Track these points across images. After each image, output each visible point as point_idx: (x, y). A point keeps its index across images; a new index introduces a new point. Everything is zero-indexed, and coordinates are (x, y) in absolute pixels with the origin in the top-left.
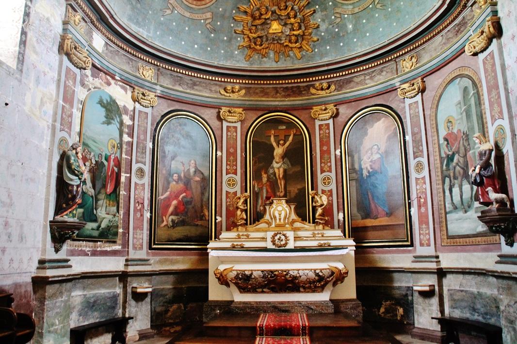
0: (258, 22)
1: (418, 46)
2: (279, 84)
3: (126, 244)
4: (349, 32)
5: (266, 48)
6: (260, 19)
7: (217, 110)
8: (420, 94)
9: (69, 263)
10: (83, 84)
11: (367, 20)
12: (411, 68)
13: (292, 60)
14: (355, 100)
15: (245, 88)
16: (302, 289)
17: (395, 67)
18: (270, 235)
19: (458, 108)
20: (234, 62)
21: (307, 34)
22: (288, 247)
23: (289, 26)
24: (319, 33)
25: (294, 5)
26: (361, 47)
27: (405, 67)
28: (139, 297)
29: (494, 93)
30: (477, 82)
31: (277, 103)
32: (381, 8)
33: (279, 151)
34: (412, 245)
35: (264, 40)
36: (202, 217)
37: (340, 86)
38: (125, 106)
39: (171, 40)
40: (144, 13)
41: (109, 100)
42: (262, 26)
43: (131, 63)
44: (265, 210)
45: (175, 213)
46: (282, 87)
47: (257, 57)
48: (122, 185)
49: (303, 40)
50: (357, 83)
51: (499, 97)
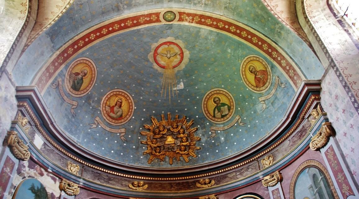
0: (158, 136)
1: (273, 149)
2: (173, 180)
4: (222, 142)
5: (163, 155)
6: (159, 134)
8: (279, 183)
10: (19, 172)
11: (234, 134)
12: (269, 165)
13: (182, 163)
14: (230, 190)
15: (148, 183)
17: (258, 165)
19: (311, 190)
20: (140, 164)
21: (192, 144)
24: (201, 144)
25: (183, 125)
26: (231, 153)
27: (265, 164)
29: (340, 176)
30: (323, 169)
31: (172, 195)
32: (243, 125)
35: (162, 149)
37: (219, 180)
38: (52, 194)
39: (94, 146)
40: (76, 125)
41: (40, 187)
42: (161, 139)
43: (62, 160)
46: (175, 183)
47: (156, 161)
49: (189, 149)
51: (346, 178)
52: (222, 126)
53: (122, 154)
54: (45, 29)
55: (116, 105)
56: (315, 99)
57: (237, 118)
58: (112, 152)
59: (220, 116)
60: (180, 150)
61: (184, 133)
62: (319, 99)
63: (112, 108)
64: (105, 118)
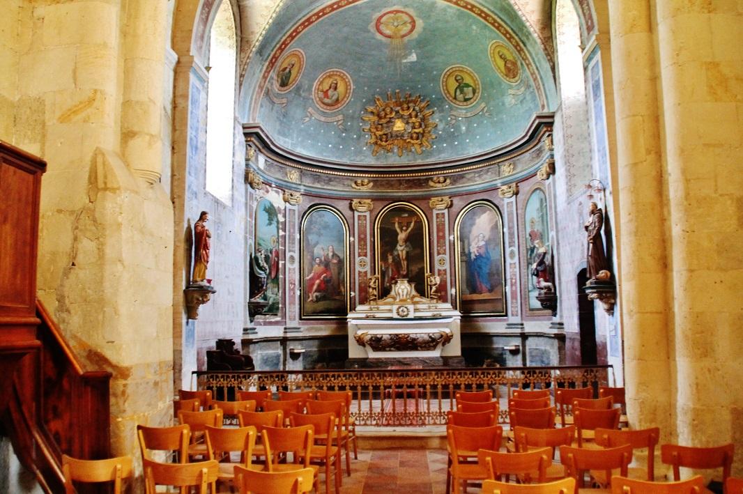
0: (383, 121)
3: (284, 316)
6: (385, 117)
7: (349, 201)
9: (256, 331)
16: (419, 348)
18: (395, 307)
22: (409, 317)
23: (411, 125)
26: (474, 150)
28: (295, 356)
31: (400, 194)
33: (402, 236)
34: (506, 315)
36: (339, 293)
37: (455, 180)
44: (391, 288)
48: (280, 271)
50: (469, 179)
52: (465, 111)
53: (341, 147)
54: (254, 49)
55: (330, 88)
56: (547, 131)
57: (483, 105)
58: (330, 146)
59: (462, 99)
60: (412, 138)
61: (416, 116)
62: (552, 131)
63: (326, 93)
64: (318, 106)
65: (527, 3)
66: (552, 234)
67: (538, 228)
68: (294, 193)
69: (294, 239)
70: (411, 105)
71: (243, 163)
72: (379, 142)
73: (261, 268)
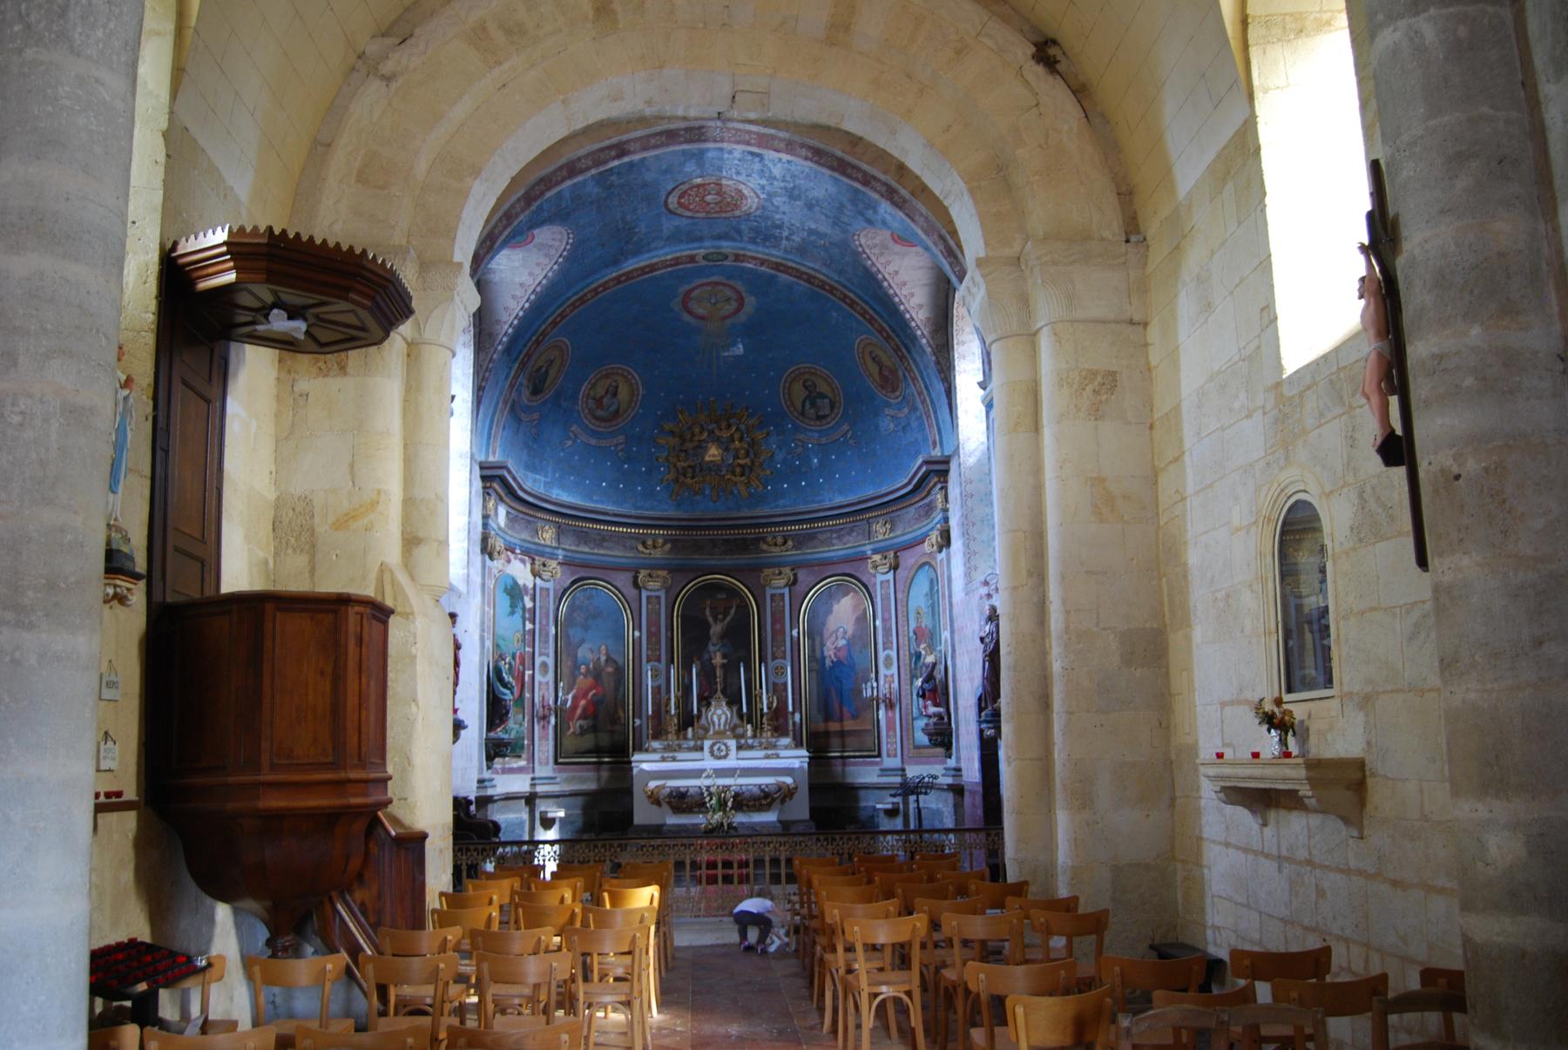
33: (716, 629)
34: (879, 755)
37: (802, 541)
45: (583, 716)
60: (733, 473)
63: (599, 401)
65: (912, 295)
66: (946, 634)
67: (926, 622)
68: (549, 562)
69: (547, 635)
70: (732, 421)
71: (480, 522)
72: (682, 478)
73: (505, 685)
